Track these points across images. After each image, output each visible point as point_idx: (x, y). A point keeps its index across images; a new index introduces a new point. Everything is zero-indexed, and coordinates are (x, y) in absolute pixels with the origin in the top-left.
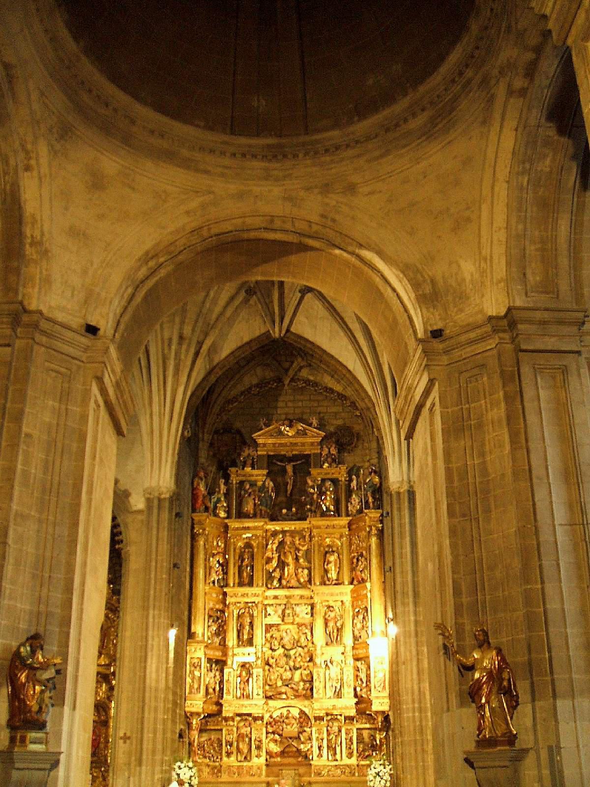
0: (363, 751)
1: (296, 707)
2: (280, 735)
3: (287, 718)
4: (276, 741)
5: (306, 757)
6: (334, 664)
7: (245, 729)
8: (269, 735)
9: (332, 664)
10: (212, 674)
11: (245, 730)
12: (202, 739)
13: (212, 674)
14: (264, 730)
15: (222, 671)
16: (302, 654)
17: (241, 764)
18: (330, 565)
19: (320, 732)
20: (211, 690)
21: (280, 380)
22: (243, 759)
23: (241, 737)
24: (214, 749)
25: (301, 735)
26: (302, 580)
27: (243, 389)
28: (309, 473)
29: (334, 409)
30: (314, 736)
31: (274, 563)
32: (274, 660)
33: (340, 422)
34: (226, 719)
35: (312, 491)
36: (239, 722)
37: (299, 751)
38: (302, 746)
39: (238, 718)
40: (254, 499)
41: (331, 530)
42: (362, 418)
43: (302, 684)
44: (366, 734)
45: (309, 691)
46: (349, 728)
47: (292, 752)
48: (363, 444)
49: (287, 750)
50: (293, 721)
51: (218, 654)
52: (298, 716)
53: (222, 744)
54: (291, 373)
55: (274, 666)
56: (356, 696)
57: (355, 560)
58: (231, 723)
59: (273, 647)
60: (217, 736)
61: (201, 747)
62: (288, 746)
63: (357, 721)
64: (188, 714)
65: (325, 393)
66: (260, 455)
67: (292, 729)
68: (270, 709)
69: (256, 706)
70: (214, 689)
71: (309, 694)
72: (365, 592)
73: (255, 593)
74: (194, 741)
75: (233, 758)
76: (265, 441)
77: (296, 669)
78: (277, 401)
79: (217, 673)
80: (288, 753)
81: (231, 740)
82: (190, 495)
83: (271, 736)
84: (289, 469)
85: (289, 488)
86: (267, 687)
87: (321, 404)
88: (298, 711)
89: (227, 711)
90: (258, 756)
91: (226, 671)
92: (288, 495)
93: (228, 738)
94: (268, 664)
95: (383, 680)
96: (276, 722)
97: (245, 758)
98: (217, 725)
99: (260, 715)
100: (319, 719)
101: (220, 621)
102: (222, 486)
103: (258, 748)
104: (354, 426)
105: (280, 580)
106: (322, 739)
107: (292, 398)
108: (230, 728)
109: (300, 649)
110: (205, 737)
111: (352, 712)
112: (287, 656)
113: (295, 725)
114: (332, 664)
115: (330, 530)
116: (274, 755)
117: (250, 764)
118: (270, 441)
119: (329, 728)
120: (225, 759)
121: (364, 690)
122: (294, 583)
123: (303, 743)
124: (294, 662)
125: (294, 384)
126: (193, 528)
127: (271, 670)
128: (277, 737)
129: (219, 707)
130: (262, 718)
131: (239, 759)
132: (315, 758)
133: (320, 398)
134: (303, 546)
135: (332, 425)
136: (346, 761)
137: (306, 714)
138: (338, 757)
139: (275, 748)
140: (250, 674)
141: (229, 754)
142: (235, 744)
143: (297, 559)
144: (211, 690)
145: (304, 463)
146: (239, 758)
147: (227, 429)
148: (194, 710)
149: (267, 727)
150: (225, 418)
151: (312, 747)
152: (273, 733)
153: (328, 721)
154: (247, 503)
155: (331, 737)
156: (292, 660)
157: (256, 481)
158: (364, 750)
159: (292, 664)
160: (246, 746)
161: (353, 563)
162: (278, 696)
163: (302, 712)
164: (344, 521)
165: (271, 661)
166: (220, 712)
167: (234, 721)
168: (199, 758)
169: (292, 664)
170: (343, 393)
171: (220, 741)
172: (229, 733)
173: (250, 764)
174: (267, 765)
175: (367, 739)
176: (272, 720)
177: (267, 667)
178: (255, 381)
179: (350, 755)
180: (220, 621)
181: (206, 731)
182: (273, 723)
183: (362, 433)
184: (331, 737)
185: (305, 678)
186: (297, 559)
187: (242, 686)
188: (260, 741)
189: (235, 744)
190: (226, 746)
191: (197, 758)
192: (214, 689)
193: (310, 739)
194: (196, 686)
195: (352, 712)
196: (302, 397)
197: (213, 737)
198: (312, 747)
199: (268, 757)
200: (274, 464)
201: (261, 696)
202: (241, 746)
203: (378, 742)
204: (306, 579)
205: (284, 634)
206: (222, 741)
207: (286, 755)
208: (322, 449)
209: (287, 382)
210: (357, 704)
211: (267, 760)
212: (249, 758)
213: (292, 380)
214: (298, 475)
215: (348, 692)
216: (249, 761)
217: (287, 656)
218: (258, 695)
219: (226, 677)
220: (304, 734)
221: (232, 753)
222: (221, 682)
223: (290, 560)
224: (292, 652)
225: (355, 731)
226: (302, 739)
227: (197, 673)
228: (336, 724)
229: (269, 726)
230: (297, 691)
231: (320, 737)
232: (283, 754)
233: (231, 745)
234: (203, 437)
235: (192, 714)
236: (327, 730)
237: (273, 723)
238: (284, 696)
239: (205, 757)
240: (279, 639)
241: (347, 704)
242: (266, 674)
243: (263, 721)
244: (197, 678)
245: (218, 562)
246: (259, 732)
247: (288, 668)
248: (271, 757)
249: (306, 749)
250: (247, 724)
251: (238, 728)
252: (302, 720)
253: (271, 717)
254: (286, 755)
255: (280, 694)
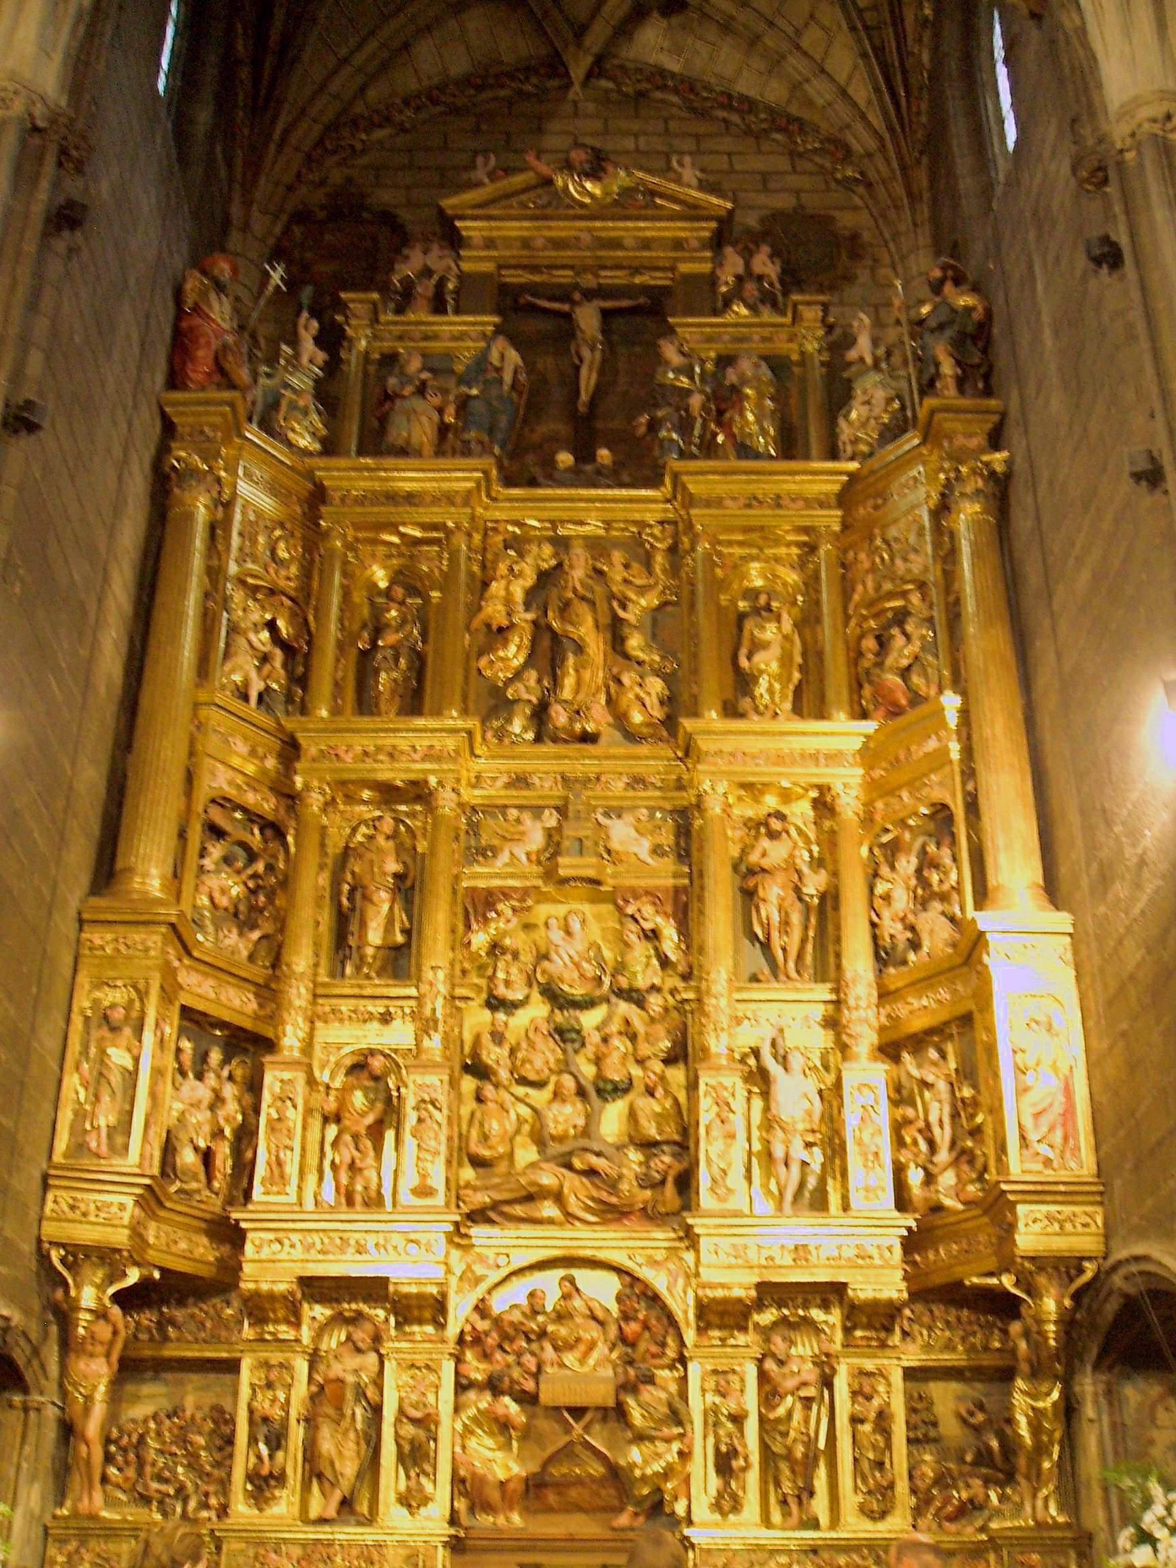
0: (939, 1481)
1: (595, 1262)
2: (528, 1399)
3: (561, 1316)
4: (503, 1426)
5: (656, 1508)
6: (796, 1061)
7: (352, 1361)
8: (472, 1395)
9: (784, 1061)
10: (203, 1092)
11: (350, 1368)
12: (140, 1411)
13: (203, 1092)
14: (448, 1367)
15: (254, 1086)
16: (639, 1025)
17: (324, 1533)
18: (759, 658)
19: (722, 1379)
20: (188, 1157)
21: (555, 66)
22: (331, 1512)
23: (326, 1395)
24: (193, 1464)
25: (630, 1401)
26: (637, 717)
27: (413, 86)
28: (670, 331)
29: (758, 163)
30: (696, 1404)
31: (514, 653)
32: (505, 1052)
33: (783, 202)
34: (259, 1308)
35: (684, 382)
36: (322, 1330)
37: (617, 1475)
38: (635, 1454)
39: (321, 1312)
40: (441, 411)
41: (762, 517)
42: (869, 185)
43: (635, 1156)
44: (946, 1399)
45: (670, 1189)
46: (869, 1365)
47: (579, 1482)
48: (873, 269)
49: (556, 1471)
50: (591, 1332)
51: (236, 1004)
52: (614, 1308)
53: (230, 1441)
54: (597, 36)
55: (504, 1074)
56: (902, 1202)
57: (870, 644)
58: (286, 1332)
59: (501, 991)
60: (209, 1399)
61: (124, 1447)
62: (566, 1453)
63: (905, 1334)
64: (55, 1256)
65: (721, 114)
66: (470, 276)
67: (585, 1373)
68: (479, 1270)
69: (410, 1253)
70: (207, 1157)
71: (676, 1189)
72: (932, 744)
73: (420, 746)
74: (87, 1410)
75: (284, 1504)
76: (494, 235)
77: (608, 1090)
78: (540, 130)
79: (229, 1091)
80: (561, 1486)
81: (277, 1413)
82: (168, 332)
83: (481, 1401)
84: (588, 318)
85: (588, 380)
86: (468, 1173)
87: (707, 144)
88: (613, 1283)
89: (269, 1264)
90: (411, 1501)
91: (272, 1080)
92: (582, 409)
93: (264, 1404)
94: (478, 1069)
95: (1058, 1108)
96: (507, 1333)
97: (346, 1504)
98: (214, 1339)
99: (434, 1290)
100: (722, 1315)
101: (260, 867)
102: (308, 346)
103: (415, 1456)
104: (837, 214)
105: (540, 714)
106: (738, 1419)
107: (598, 125)
108: (276, 1357)
109: (624, 1008)
110: (147, 1402)
111: (886, 1283)
112: (564, 1035)
113: (601, 1349)
114: (784, 1061)
115: (758, 515)
116: (495, 1496)
117: (367, 1535)
118: (515, 229)
119: (770, 1365)
120: (241, 1508)
121: (948, 1179)
122: (598, 719)
123: (640, 1438)
124: (598, 1061)
125: (605, 84)
126: (163, 450)
127: (489, 1091)
128: (510, 1407)
129: (226, 1249)
130: (437, 1308)
131: (315, 1511)
132: (702, 1510)
133: (702, 128)
134: (642, 590)
135: (751, 208)
136: (855, 1527)
137: (654, 1299)
138: (820, 1505)
139: (501, 1464)
140: (390, 1111)
141: (263, 1485)
142: (297, 1434)
143: (616, 633)
144: (188, 1157)
145: (642, 315)
146: (316, 1507)
147: (346, 207)
148: (87, 1234)
149: (459, 1360)
150: (337, 176)
151: (684, 1455)
152: (494, 1386)
153: (766, 1332)
154: (411, 414)
155: (781, 1411)
156: (590, 1050)
157: (449, 356)
158: (940, 1480)
159: (588, 1071)
160: (350, 1448)
161: (860, 654)
162: (518, 1210)
163: (638, 1293)
164: (820, 478)
165: (493, 1055)
166: (230, 1270)
167: (297, 1325)
168: (110, 1502)
169: (588, 1071)
170: (794, 110)
171: (222, 1419)
172: (272, 1378)
173: (367, 1535)
174: (456, 1546)
175: (950, 1428)
176: (483, 1325)
177: (469, 1084)
178: (459, 65)
179: (879, 1503)
180: (260, 867)
181: (161, 1367)
182: (492, 1340)
183: (866, 236)
184: (781, 1411)
185: (652, 1131)
186: (616, 633)
187: (347, 1154)
188: (426, 1423)
189: (297, 1434)
190: (253, 1440)
191: (98, 1496)
192: (207, 1157)
193: (676, 1416)
194: (106, 1117)
195: (886, 1283)
196: (636, 126)
197: (190, 1402)
198: (684, 1455)
199: (461, 1505)
200: (528, 309)
201: (440, 1200)
202: (326, 1445)
203: (1024, 1431)
204: (658, 713)
205: (557, 935)
206: (232, 1421)
207: (552, 1498)
208: (718, 261)
209: (578, 71)
210: (912, 1243)
211: (453, 1520)
212: (363, 1508)
213: (597, 69)
214: (622, 350)
215: (869, 1180)
216: (370, 1520)
217: (564, 1035)
218: (424, 1191)
219: (267, 1110)
220: (649, 1394)
221: (280, 1478)
222: (245, 1135)
223: (586, 629)
224: (589, 1020)
225: (897, 1377)
226: (637, 1416)
227: (119, 1057)
228: (804, 1348)
229: (469, 1355)
230: (613, 1185)
231: (731, 1405)
232: (535, 1491)
233: (277, 1441)
234: (247, 215)
235: (77, 1255)
236: (763, 1376)
237: (492, 1340)
238: (549, 1209)
239: (145, 1500)
240: (527, 958)
241: (865, 1248)
242: (465, 1111)
243: (441, 1326)
244: (116, 1078)
245: (271, 626)
246: (414, 1375)
247: (568, 1082)
248: (479, 1504)
249: (657, 1467)
250: (362, 1335)
251: (314, 1359)
252: (632, 1328)
253: (481, 1309)
254: (552, 1498)
255: (529, 1198)
